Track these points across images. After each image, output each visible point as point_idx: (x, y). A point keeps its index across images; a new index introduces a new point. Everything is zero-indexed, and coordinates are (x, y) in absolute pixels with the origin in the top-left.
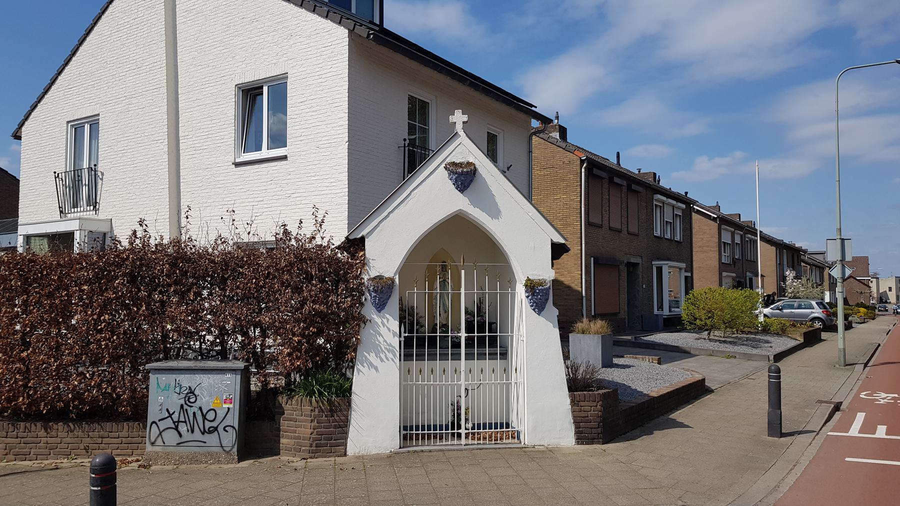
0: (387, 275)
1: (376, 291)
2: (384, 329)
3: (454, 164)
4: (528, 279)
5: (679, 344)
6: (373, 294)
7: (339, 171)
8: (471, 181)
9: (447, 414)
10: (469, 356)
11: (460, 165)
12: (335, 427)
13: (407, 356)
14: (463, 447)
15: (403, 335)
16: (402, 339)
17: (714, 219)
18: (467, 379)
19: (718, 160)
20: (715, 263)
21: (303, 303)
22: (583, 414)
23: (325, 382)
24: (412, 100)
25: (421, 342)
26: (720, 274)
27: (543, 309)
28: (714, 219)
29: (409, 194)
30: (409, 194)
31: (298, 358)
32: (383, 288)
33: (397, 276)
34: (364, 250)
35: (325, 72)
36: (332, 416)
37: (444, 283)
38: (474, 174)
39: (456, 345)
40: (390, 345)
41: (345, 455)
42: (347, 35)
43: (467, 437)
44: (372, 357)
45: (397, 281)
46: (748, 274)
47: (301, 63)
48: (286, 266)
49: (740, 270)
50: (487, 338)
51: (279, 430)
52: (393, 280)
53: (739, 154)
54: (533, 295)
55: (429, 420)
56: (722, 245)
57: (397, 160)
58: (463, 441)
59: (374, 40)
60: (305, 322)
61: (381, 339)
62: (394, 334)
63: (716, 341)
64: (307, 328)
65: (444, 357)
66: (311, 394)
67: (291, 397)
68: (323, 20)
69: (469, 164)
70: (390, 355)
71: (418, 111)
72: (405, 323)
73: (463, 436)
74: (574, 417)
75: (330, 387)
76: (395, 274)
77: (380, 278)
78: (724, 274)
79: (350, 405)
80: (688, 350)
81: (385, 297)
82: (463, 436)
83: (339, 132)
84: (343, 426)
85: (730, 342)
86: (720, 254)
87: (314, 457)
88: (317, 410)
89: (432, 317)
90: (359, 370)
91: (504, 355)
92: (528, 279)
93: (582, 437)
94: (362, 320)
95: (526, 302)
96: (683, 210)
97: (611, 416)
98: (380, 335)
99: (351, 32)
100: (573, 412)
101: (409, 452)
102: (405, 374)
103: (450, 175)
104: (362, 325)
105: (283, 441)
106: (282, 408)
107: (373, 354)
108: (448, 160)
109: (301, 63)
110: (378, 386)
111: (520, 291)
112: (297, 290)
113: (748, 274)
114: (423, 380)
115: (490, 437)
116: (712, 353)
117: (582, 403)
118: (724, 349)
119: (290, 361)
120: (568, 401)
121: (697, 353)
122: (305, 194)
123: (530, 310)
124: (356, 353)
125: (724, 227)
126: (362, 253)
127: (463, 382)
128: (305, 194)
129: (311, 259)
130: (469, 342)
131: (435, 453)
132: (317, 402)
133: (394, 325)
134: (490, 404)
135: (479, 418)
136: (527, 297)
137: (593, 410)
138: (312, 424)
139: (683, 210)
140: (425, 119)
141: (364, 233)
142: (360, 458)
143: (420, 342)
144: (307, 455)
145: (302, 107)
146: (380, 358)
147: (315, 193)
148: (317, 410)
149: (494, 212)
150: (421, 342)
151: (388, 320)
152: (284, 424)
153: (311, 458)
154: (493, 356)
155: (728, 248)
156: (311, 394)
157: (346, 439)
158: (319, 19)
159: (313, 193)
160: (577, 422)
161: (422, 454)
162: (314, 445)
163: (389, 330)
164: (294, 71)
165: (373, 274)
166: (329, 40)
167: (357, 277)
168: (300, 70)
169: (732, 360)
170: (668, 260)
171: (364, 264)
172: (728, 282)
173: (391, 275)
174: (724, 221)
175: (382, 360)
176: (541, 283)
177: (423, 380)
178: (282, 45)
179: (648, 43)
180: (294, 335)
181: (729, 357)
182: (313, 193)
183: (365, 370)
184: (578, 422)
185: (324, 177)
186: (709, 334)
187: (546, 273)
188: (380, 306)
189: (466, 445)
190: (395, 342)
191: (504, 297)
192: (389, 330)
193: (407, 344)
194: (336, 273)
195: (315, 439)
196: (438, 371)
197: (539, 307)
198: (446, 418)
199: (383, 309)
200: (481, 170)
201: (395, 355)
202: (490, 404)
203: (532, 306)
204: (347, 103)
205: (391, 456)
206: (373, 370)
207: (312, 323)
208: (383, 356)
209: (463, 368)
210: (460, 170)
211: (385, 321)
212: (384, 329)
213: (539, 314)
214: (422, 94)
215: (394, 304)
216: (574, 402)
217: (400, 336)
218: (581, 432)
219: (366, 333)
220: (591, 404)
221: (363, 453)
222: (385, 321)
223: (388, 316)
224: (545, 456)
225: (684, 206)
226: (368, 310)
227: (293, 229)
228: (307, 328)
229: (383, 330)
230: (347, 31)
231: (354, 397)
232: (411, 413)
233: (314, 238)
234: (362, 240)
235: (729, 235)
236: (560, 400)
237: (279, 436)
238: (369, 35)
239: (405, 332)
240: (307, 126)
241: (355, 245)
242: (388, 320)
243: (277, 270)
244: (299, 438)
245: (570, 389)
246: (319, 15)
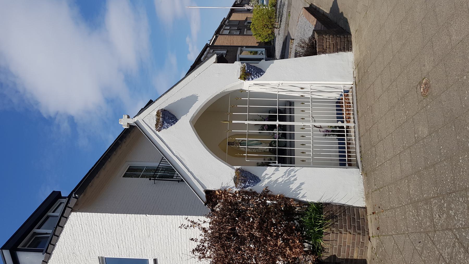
0: (234, 174)
1: (245, 182)
2: (273, 177)
3: (157, 125)
4: (241, 78)
5: (281, 43)
6: (247, 184)
7: (166, 221)
8: (170, 113)
9: (332, 139)
10: (292, 119)
11: (158, 120)
12: (345, 215)
13: (292, 162)
14: (357, 125)
15: (277, 164)
16: (280, 165)
17: (216, 37)
18: (309, 121)
19: (190, 49)
20: (240, 37)
21: (252, 236)
22: (332, 47)
23: (311, 222)
24: (125, 176)
25: (282, 152)
26: (245, 35)
27: (260, 69)
28: (216, 37)
29: (176, 156)
30: (176, 156)
31: (294, 242)
32: (243, 177)
33: (235, 167)
34: (215, 191)
35: (99, 230)
36: (337, 216)
37: (242, 143)
38: (165, 110)
39: (283, 128)
40: (285, 173)
41: (365, 208)
42: (75, 213)
43: (348, 122)
44: (294, 186)
45: (238, 167)
46: (245, 24)
47: (92, 247)
48: (224, 250)
49: (242, 28)
50: (281, 111)
51: (347, 260)
52: (237, 170)
53: (188, 39)
54: (251, 74)
55: (335, 152)
56: (230, 34)
57: (165, 186)
58: (351, 125)
59: (80, 194)
60: (266, 236)
61: (280, 180)
62: (277, 170)
63: (280, 24)
64: (271, 235)
65: (292, 136)
66: (320, 233)
67: (323, 250)
68: (65, 230)
69: (158, 115)
70: (292, 173)
71: (133, 172)
72: (270, 163)
73: (348, 124)
74: (334, 52)
75: (315, 219)
76: (233, 168)
77: (236, 180)
78: (245, 33)
79: (329, 204)
80: (285, 37)
81: (249, 175)
82: (348, 124)
83: (139, 221)
84: (344, 209)
85: (281, 18)
86: (235, 35)
87: (368, 232)
88: (333, 229)
89: (264, 152)
90: (303, 196)
91: (291, 104)
92: (241, 78)
93: (347, 47)
94: (266, 194)
95: (256, 81)
96: (210, 49)
97: (332, 32)
98: (277, 180)
99: (73, 210)
100: (330, 52)
101: (361, 162)
102: (304, 163)
103: (164, 128)
104: (270, 193)
105: (355, 257)
106: (331, 256)
107: (291, 186)
108: (154, 129)
109: (92, 247)
110: (316, 183)
111: (249, 85)
112: (242, 241)
113: (245, 24)
114: (310, 151)
115: (348, 110)
116: (287, 24)
117: (325, 47)
118: (285, 18)
119: (296, 248)
120: (323, 55)
121: (287, 32)
122: (180, 247)
123: (261, 78)
124: (290, 199)
125: (221, 33)
126: (217, 193)
127: (311, 124)
128: (180, 247)
129: (219, 230)
130: (282, 119)
131: (362, 143)
132: (326, 228)
133: (269, 170)
134: (326, 110)
135: (333, 118)
136: (252, 79)
137: (329, 40)
138: (343, 232)
139: (210, 49)
140: (139, 169)
141: (202, 190)
142: (367, 197)
143: (282, 154)
144: (366, 237)
145: (122, 247)
146: (293, 181)
147: (180, 239)
148: (333, 229)
149: (193, 99)
150: (282, 152)
151: (266, 174)
152: (343, 255)
153: (368, 234)
154: (291, 111)
155: (232, 32)
156: (320, 233)
157: (353, 207)
158: (63, 233)
159: (180, 241)
160: (337, 50)
161: (363, 152)
162: (358, 231)
163: (273, 174)
164: (98, 252)
165: (232, 184)
166: (78, 226)
167: (234, 196)
168: (97, 248)
169: (291, 13)
170: (236, 56)
171: (224, 192)
172: (249, 32)
173: (234, 171)
174: (218, 32)
175: (295, 180)
176: (243, 69)
177: (310, 151)
178: (80, 260)
179: (128, 80)
180: (276, 245)
181: (289, 15)
182: (180, 241)
183: (302, 193)
184: (337, 49)
185: (169, 233)
186: (276, 28)
187: (236, 67)
188: (256, 180)
189: (354, 122)
190: (283, 170)
191: (252, 103)
192: (273, 174)
193: (283, 161)
194: (230, 211)
195: (355, 231)
196: (303, 141)
197: (260, 72)
198: (334, 140)
199: (258, 178)
200: (163, 107)
201: (293, 170)
202: (326, 110)
203: (259, 77)
204: (120, 215)
205: (365, 173)
206: (303, 186)
207: (268, 230)
208: (293, 179)
209: (301, 124)
210: (161, 119)
211: (267, 176)
212: (273, 177)
213: (264, 72)
214: (124, 169)
215: (254, 170)
216: (324, 52)
217: (278, 166)
218: (344, 48)
219: (276, 191)
220: (325, 41)
221: (363, 195)
222: (267, 176)
223: (263, 175)
224: (361, 70)
225: (208, 48)
226: (259, 188)
227: (194, 245)
228: (271, 235)
229: (274, 178)
230: (72, 213)
231: (323, 201)
232: (331, 160)
233: (204, 229)
234: (209, 193)
235: (225, 31)
236: (322, 60)
237: (352, 260)
238: (76, 197)
239: (275, 163)
240: (134, 244)
241: (211, 197)
242: (266, 174)
243: (226, 256)
244: (353, 244)
245: (315, 54)
246: (61, 232)
